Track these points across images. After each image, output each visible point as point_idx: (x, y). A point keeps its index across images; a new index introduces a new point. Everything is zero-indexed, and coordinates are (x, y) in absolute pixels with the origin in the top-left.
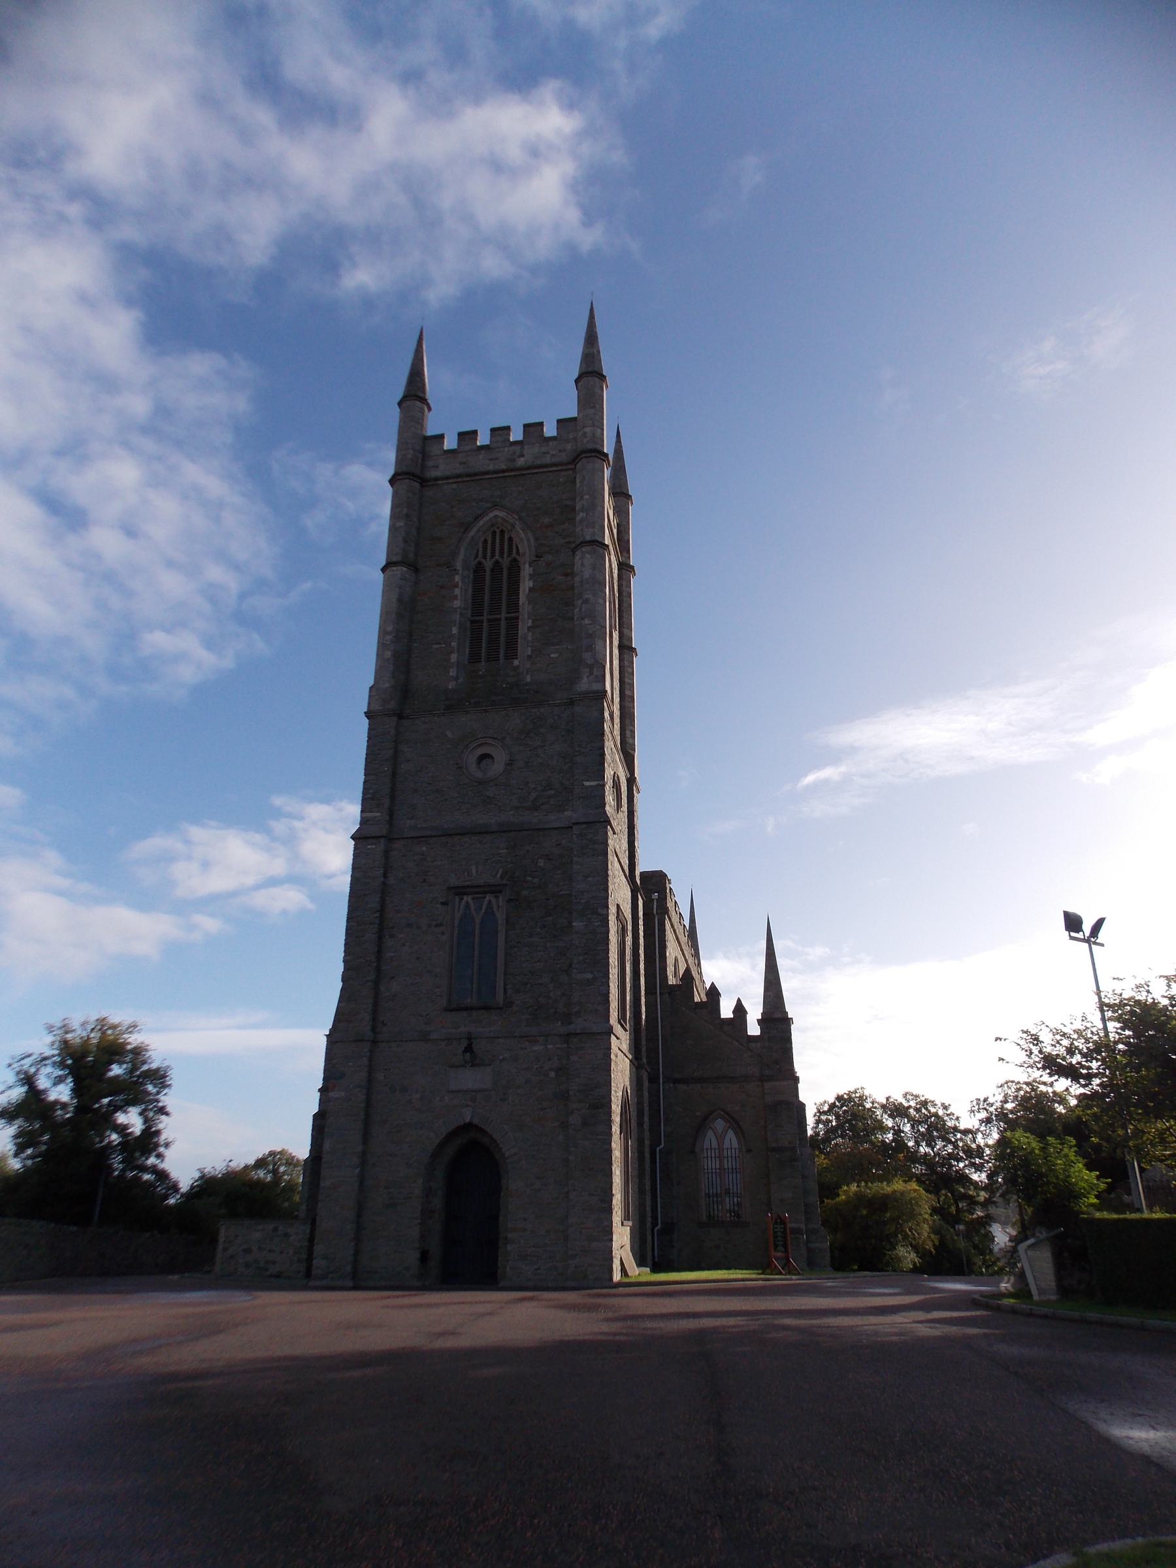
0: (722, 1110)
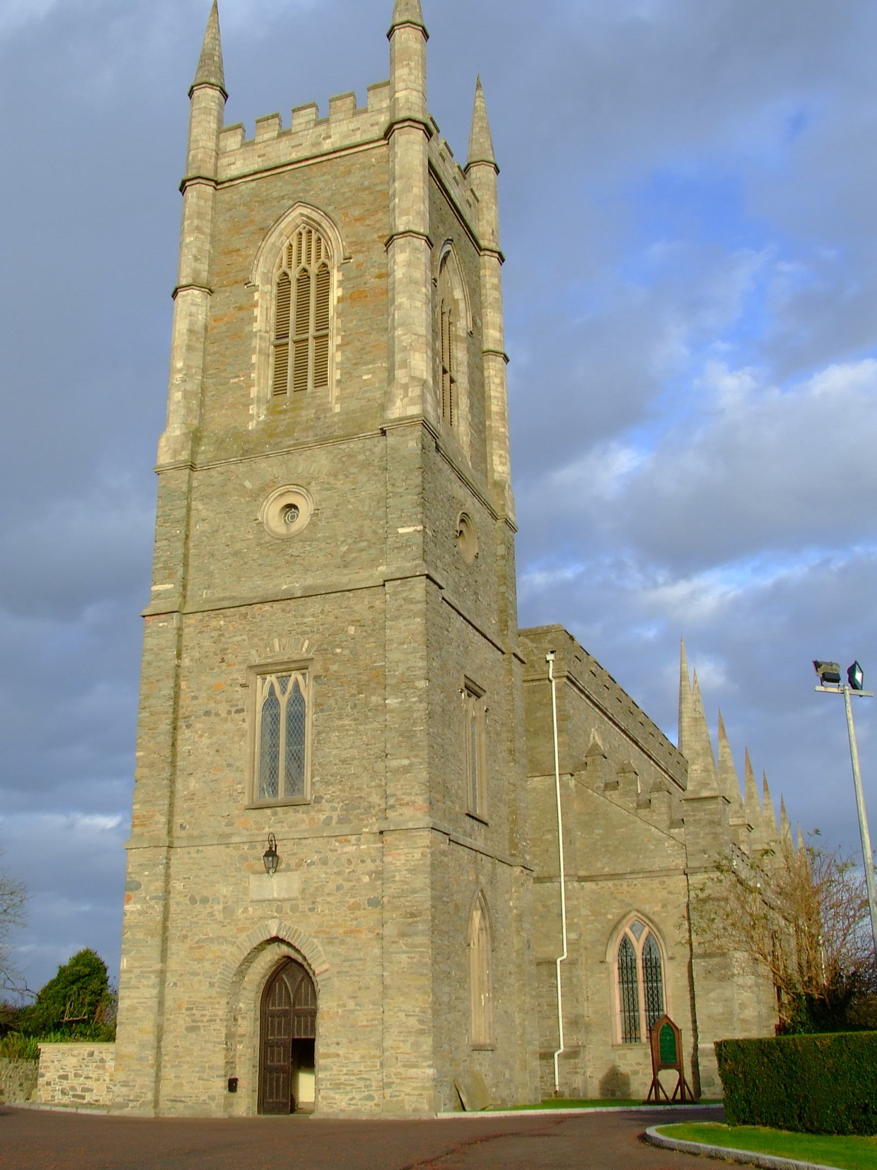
0: (638, 911)
